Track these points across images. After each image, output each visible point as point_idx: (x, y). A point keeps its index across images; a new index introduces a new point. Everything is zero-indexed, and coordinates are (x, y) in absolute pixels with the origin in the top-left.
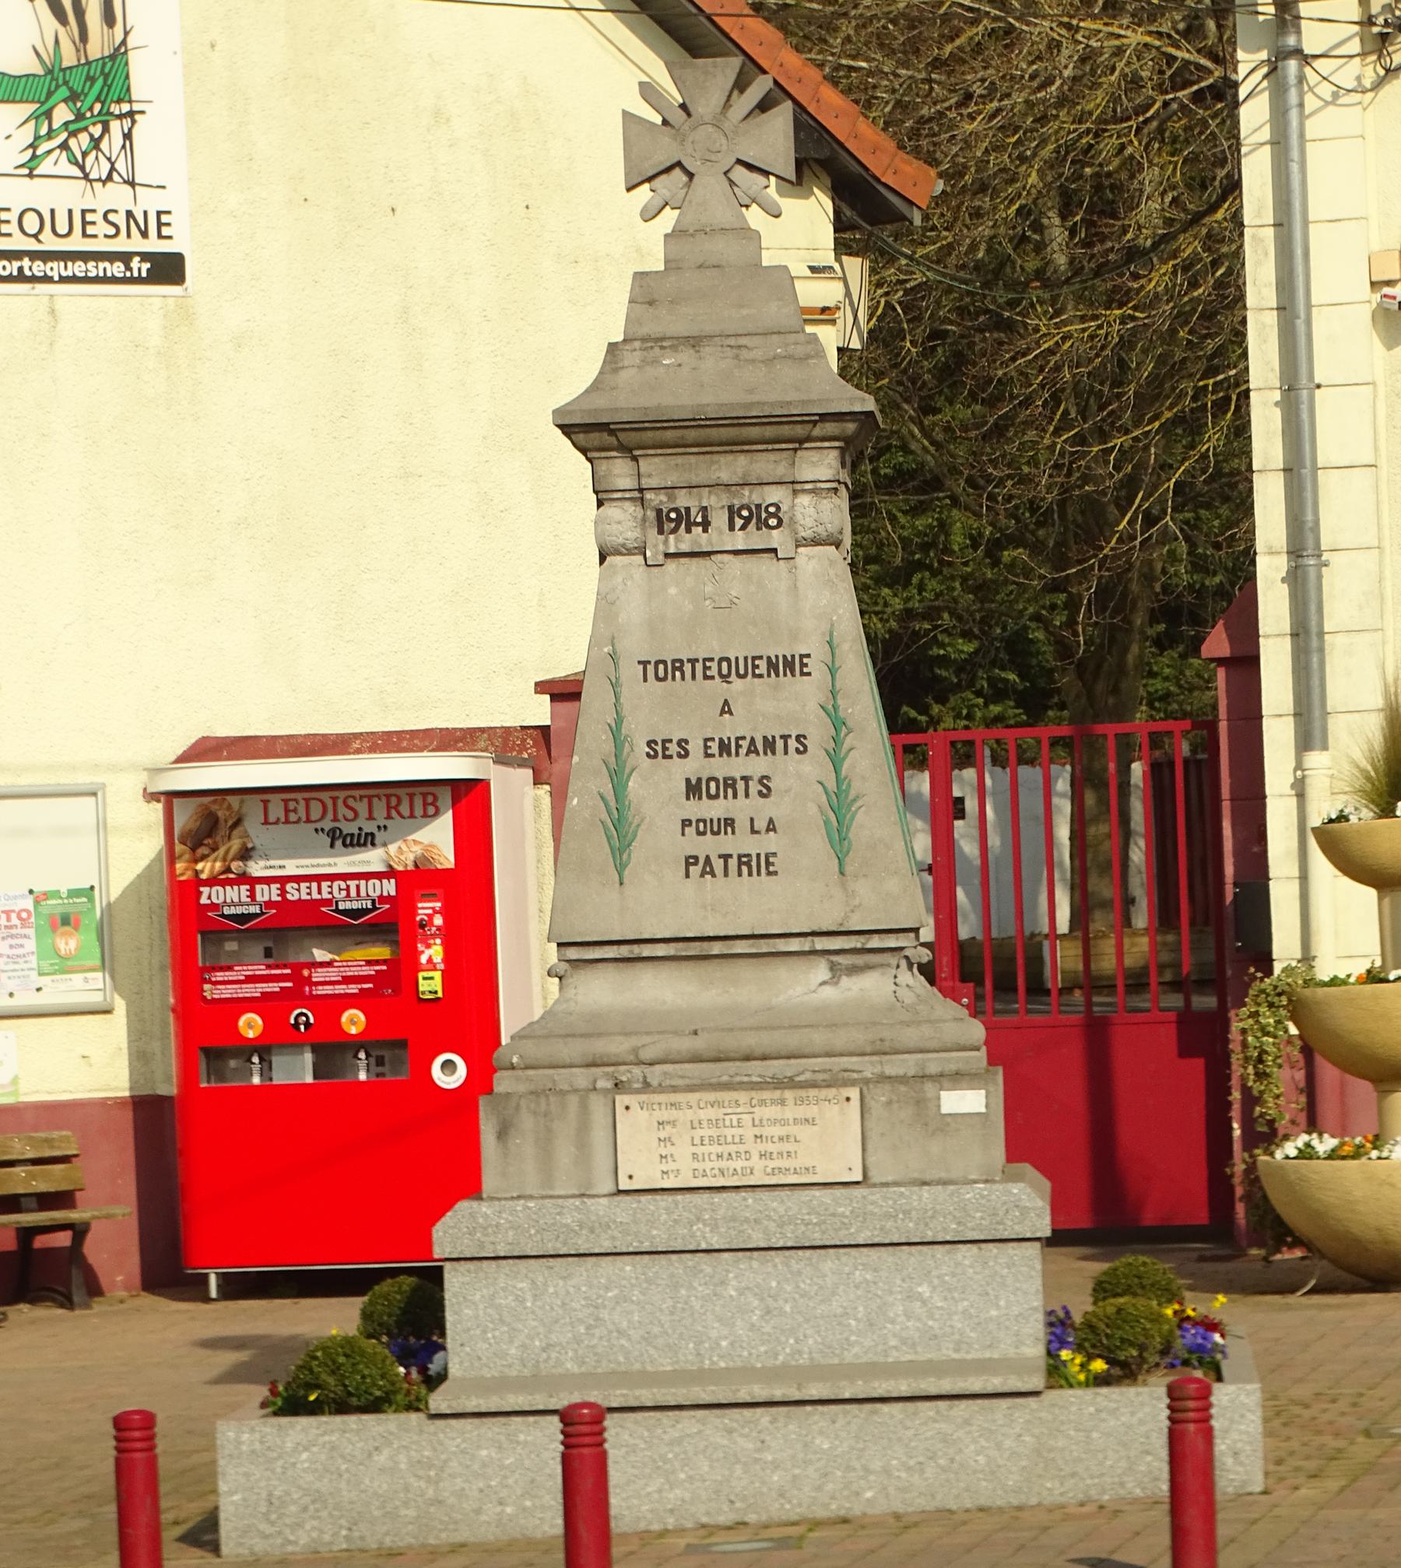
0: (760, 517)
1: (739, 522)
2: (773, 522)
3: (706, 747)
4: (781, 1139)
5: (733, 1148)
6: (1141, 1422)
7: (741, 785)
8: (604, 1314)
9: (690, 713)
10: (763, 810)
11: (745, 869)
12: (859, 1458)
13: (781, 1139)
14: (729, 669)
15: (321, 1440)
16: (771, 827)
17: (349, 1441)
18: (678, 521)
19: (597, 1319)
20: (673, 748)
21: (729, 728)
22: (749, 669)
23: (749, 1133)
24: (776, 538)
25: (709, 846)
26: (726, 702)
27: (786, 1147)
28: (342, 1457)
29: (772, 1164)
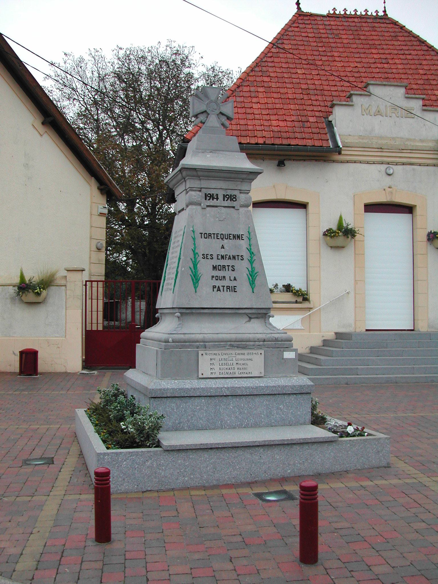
0: (232, 198)
1: (226, 199)
2: (234, 200)
3: (218, 257)
4: (243, 364)
5: (230, 367)
6: (361, 448)
7: (227, 267)
8: (196, 413)
9: (214, 246)
10: (233, 274)
11: (228, 290)
12: (287, 461)
13: (243, 364)
14: (223, 237)
15: (130, 458)
16: (235, 279)
17: (138, 458)
18: (210, 197)
19: (194, 415)
20: (209, 257)
21: (223, 252)
22: (228, 237)
23: (235, 362)
24: (234, 204)
25: (218, 283)
26: (223, 245)
27: (244, 366)
28: (136, 463)
29: (241, 371)
